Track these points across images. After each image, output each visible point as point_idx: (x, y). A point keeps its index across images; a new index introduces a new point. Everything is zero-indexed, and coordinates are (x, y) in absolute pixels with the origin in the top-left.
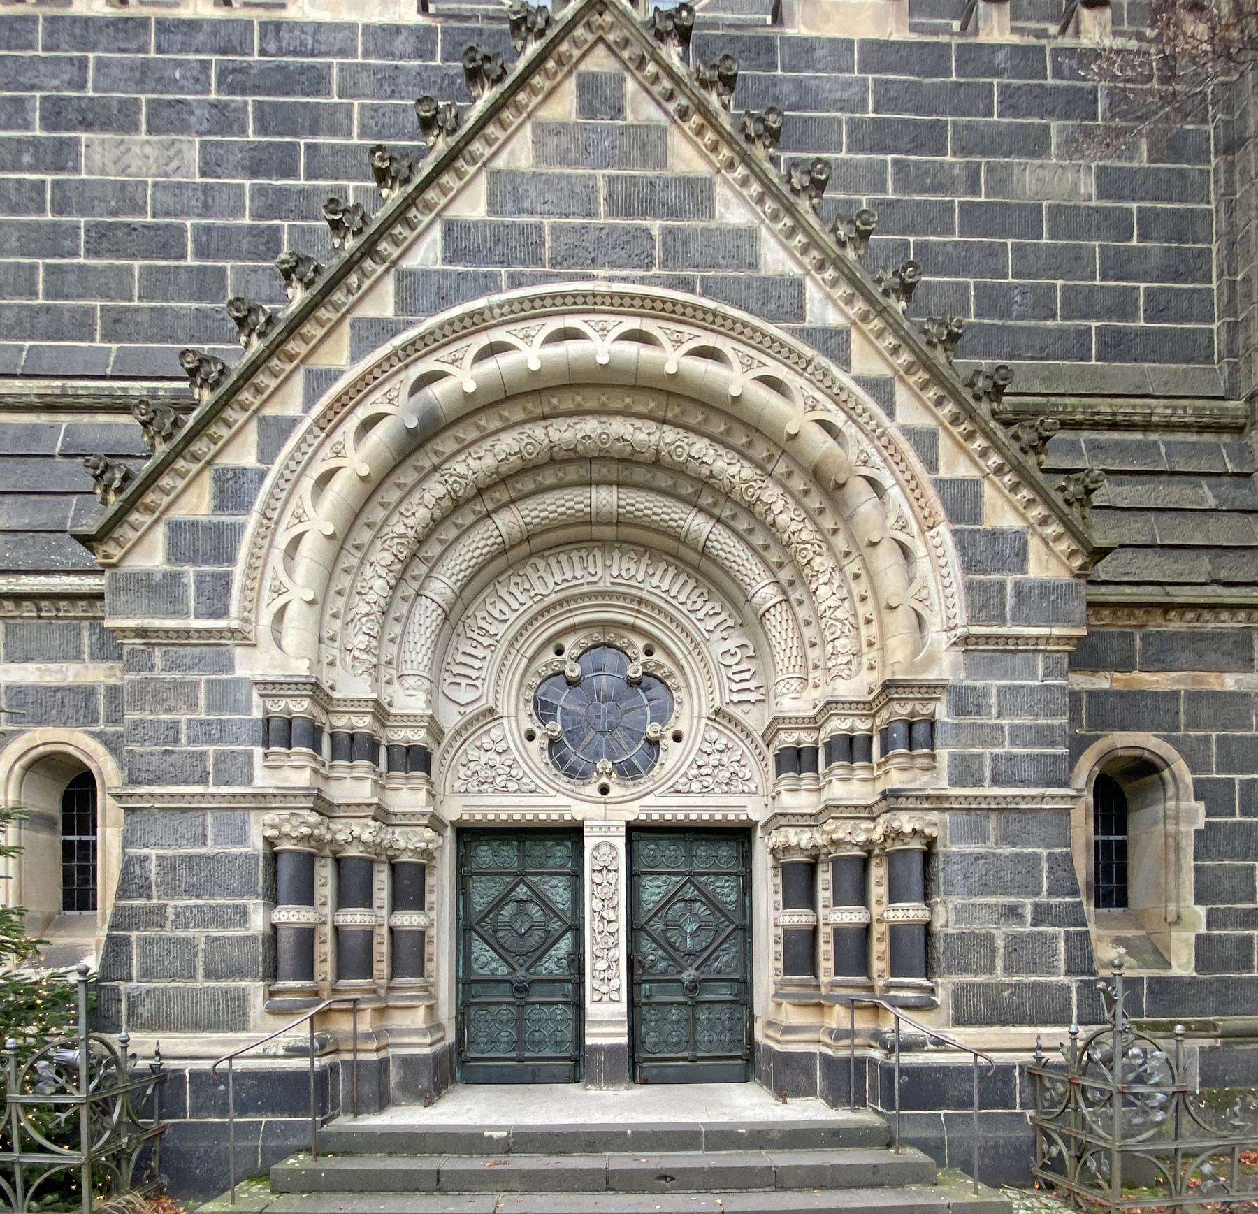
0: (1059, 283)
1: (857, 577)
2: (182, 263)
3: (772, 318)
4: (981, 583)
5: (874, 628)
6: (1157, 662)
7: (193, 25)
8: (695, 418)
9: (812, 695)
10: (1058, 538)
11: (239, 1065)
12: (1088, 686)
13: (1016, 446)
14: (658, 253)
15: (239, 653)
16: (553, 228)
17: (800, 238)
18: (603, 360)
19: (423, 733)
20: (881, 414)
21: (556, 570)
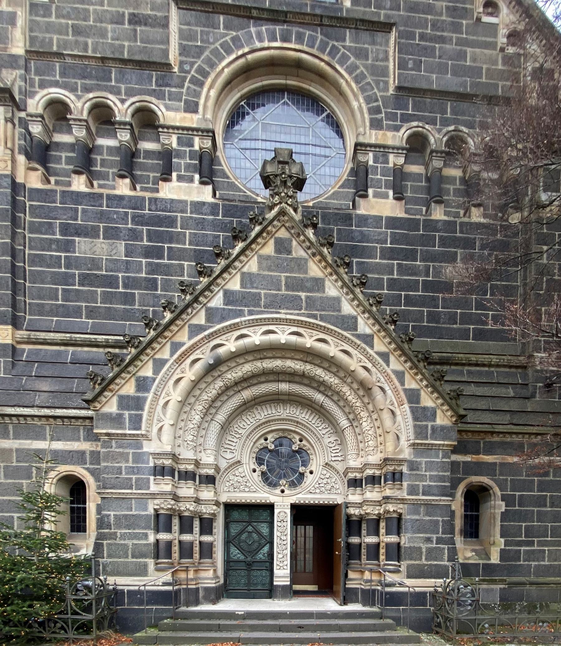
0: (459, 311)
1: (376, 420)
2: (118, 290)
3: (345, 330)
4: (419, 425)
5: (382, 438)
6: (488, 452)
7: (121, 198)
8: (318, 362)
9: (360, 460)
10: (447, 411)
11: (148, 588)
12: (463, 460)
13: (433, 378)
14: (304, 304)
15: (145, 443)
16: (265, 294)
17: (356, 302)
18: (283, 341)
19: (213, 470)
20: (384, 365)
21: (265, 411)
